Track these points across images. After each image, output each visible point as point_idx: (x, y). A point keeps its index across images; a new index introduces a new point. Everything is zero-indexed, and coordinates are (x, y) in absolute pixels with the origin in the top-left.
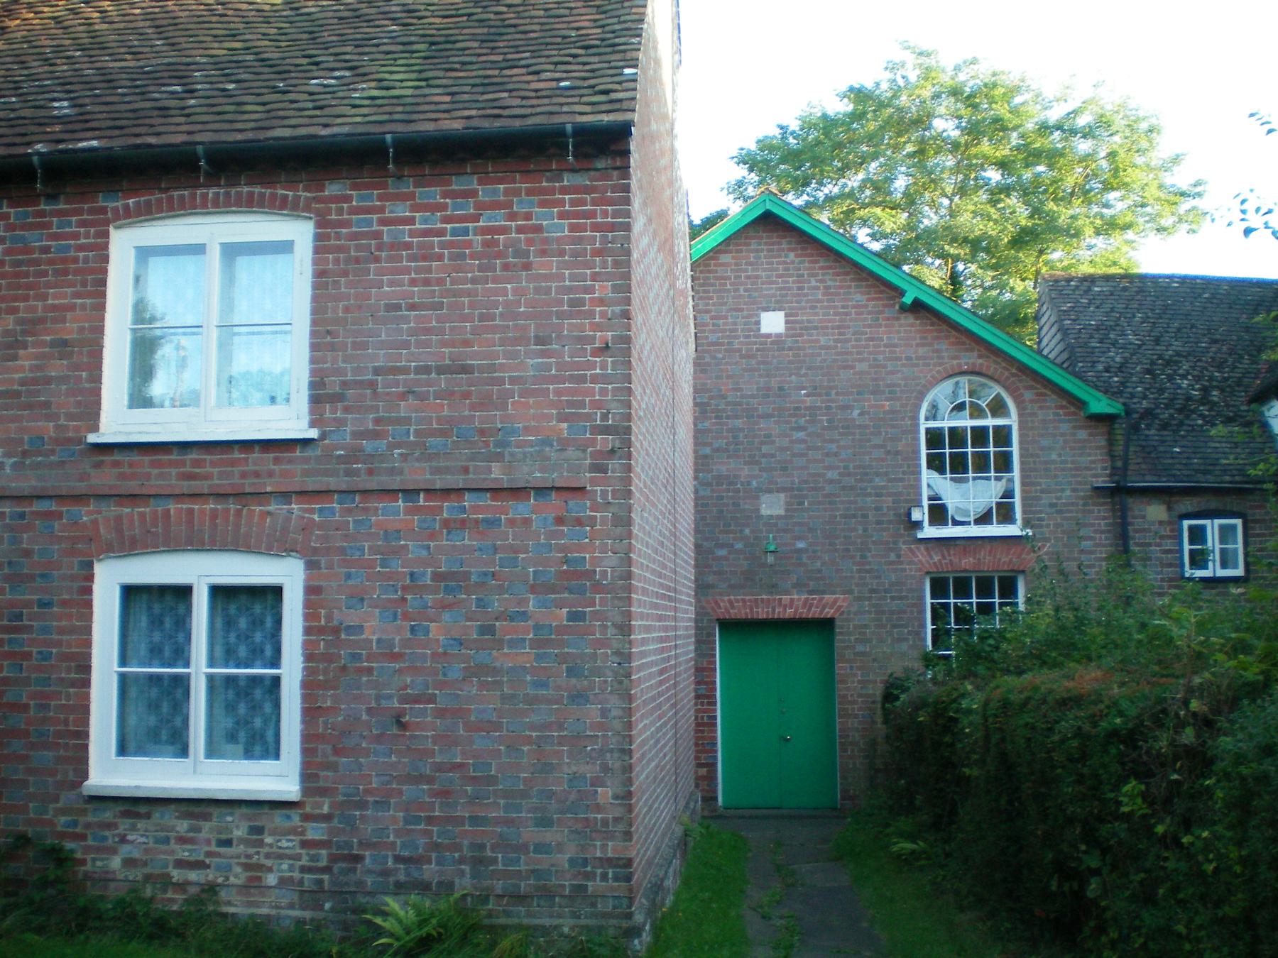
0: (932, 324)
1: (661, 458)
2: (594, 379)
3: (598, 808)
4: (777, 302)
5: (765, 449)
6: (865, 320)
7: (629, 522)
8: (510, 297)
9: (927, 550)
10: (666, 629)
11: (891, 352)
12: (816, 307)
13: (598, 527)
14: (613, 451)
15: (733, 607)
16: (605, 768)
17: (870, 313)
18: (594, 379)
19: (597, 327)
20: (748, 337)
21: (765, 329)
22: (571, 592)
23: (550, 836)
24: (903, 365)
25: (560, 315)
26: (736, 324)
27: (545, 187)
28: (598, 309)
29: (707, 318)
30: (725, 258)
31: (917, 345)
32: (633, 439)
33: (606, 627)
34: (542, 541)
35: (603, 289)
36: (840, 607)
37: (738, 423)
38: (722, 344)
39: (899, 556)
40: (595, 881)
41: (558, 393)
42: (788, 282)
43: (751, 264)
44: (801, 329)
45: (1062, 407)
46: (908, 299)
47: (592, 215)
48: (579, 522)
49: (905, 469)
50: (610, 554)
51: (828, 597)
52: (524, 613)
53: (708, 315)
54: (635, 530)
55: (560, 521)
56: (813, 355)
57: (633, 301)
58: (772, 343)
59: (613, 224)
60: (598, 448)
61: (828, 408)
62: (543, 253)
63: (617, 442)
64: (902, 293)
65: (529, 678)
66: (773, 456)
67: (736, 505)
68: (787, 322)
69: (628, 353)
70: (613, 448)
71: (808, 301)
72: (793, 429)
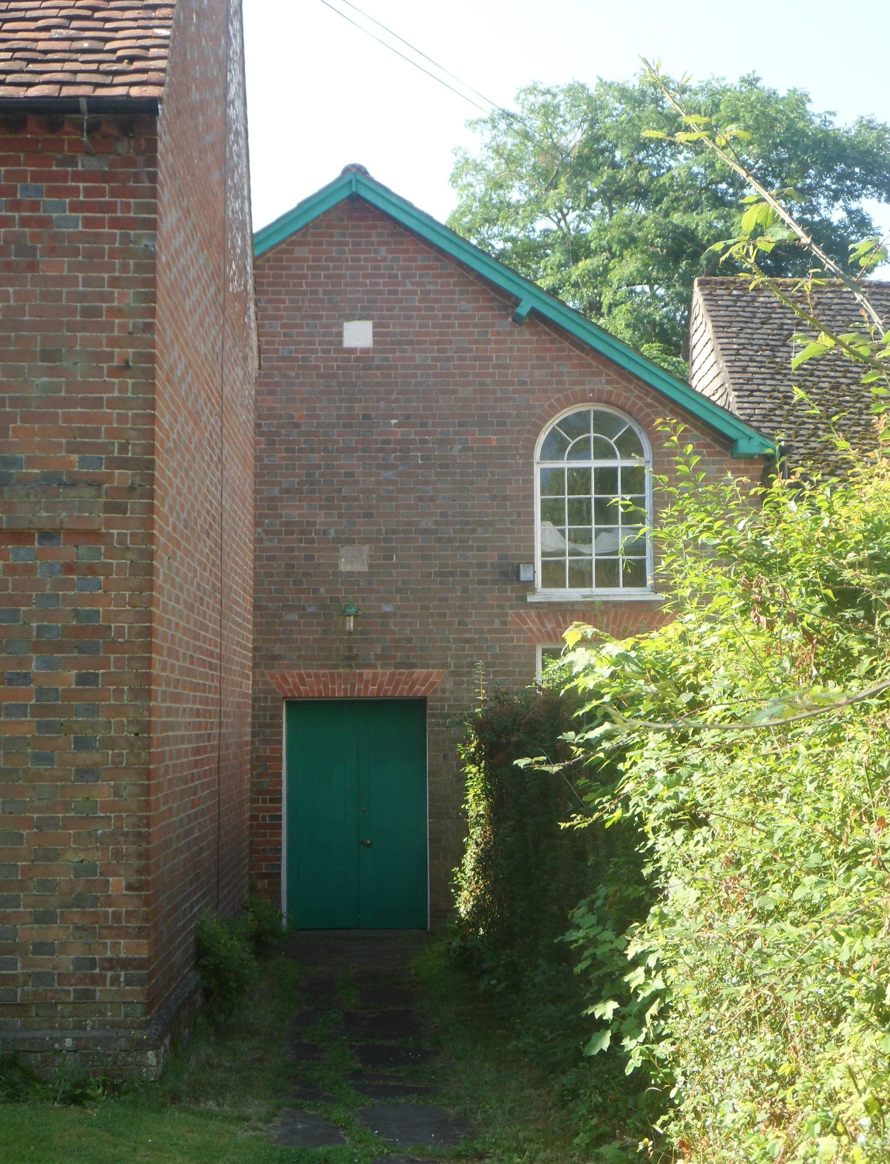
0: (552, 341)
1: (200, 498)
2: (112, 402)
3: (109, 901)
4: (364, 309)
5: (346, 491)
6: (471, 334)
7: (150, 570)
8: (12, 302)
9: (539, 615)
10: (205, 701)
11: (501, 375)
12: (411, 317)
13: (114, 576)
14: (132, 488)
15: (303, 683)
16: (117, 854)
17: (476, 326)
18: (112, 402)
19: (112, 342)
20: (328, 351)
21: (348, 343)
22: (81, 651)
23: (55, 933)
24: (515, 391)
25: (71, 327)
26: (312, 334)
27: (54, 172)
28: (117, 321)
29: (277, 327)
30: (302, 252)
31: (534, 367)
32: (156, 474)
33: (122, 692)
34: (48, 592)
35: (127, 298)
36: (434, 683)
37: (316, 458)
38: (296, 360)
39: (504, 623)
40: (105, 985)
41: (68, 418)
42: (378, 284)
43: (332, 260)
44: (393, 343)
45: (707, 446)
46: (523, 310)
47: (111, 207)
48: (92, 570)
49: (515, 518)
50: (128, 607)
51: (420, 672)
52: (26, 675)
53: (279, 323)
54: (159, 581)
55: (69, 568)
56: (406, 376)
57: (159, 313)
58: (357, 359)
59: (133, 220)
60: (116, 484)
61: (423, 442)
62: (52, 251)
63: (138, 478)
64: (517, 302)
65: (29, 751)
66: (355, 499)
67: (309, 558)
68: (375, 334)
69: (151, 374)
70: (133, 484)
71: (402, 309)
72: (379, 466)
